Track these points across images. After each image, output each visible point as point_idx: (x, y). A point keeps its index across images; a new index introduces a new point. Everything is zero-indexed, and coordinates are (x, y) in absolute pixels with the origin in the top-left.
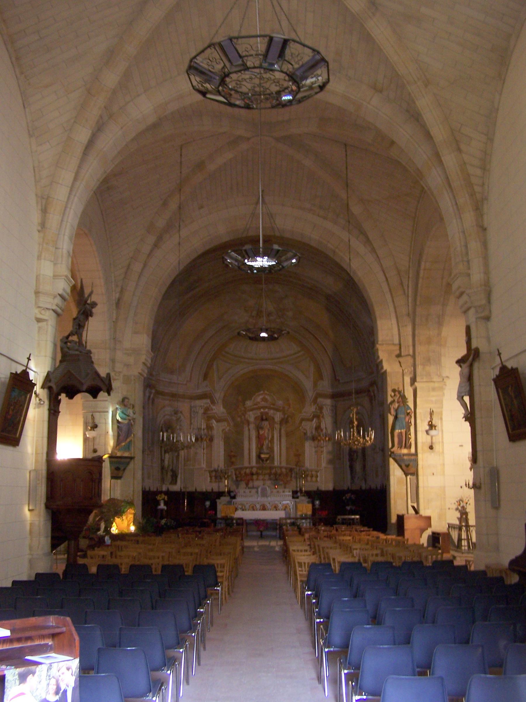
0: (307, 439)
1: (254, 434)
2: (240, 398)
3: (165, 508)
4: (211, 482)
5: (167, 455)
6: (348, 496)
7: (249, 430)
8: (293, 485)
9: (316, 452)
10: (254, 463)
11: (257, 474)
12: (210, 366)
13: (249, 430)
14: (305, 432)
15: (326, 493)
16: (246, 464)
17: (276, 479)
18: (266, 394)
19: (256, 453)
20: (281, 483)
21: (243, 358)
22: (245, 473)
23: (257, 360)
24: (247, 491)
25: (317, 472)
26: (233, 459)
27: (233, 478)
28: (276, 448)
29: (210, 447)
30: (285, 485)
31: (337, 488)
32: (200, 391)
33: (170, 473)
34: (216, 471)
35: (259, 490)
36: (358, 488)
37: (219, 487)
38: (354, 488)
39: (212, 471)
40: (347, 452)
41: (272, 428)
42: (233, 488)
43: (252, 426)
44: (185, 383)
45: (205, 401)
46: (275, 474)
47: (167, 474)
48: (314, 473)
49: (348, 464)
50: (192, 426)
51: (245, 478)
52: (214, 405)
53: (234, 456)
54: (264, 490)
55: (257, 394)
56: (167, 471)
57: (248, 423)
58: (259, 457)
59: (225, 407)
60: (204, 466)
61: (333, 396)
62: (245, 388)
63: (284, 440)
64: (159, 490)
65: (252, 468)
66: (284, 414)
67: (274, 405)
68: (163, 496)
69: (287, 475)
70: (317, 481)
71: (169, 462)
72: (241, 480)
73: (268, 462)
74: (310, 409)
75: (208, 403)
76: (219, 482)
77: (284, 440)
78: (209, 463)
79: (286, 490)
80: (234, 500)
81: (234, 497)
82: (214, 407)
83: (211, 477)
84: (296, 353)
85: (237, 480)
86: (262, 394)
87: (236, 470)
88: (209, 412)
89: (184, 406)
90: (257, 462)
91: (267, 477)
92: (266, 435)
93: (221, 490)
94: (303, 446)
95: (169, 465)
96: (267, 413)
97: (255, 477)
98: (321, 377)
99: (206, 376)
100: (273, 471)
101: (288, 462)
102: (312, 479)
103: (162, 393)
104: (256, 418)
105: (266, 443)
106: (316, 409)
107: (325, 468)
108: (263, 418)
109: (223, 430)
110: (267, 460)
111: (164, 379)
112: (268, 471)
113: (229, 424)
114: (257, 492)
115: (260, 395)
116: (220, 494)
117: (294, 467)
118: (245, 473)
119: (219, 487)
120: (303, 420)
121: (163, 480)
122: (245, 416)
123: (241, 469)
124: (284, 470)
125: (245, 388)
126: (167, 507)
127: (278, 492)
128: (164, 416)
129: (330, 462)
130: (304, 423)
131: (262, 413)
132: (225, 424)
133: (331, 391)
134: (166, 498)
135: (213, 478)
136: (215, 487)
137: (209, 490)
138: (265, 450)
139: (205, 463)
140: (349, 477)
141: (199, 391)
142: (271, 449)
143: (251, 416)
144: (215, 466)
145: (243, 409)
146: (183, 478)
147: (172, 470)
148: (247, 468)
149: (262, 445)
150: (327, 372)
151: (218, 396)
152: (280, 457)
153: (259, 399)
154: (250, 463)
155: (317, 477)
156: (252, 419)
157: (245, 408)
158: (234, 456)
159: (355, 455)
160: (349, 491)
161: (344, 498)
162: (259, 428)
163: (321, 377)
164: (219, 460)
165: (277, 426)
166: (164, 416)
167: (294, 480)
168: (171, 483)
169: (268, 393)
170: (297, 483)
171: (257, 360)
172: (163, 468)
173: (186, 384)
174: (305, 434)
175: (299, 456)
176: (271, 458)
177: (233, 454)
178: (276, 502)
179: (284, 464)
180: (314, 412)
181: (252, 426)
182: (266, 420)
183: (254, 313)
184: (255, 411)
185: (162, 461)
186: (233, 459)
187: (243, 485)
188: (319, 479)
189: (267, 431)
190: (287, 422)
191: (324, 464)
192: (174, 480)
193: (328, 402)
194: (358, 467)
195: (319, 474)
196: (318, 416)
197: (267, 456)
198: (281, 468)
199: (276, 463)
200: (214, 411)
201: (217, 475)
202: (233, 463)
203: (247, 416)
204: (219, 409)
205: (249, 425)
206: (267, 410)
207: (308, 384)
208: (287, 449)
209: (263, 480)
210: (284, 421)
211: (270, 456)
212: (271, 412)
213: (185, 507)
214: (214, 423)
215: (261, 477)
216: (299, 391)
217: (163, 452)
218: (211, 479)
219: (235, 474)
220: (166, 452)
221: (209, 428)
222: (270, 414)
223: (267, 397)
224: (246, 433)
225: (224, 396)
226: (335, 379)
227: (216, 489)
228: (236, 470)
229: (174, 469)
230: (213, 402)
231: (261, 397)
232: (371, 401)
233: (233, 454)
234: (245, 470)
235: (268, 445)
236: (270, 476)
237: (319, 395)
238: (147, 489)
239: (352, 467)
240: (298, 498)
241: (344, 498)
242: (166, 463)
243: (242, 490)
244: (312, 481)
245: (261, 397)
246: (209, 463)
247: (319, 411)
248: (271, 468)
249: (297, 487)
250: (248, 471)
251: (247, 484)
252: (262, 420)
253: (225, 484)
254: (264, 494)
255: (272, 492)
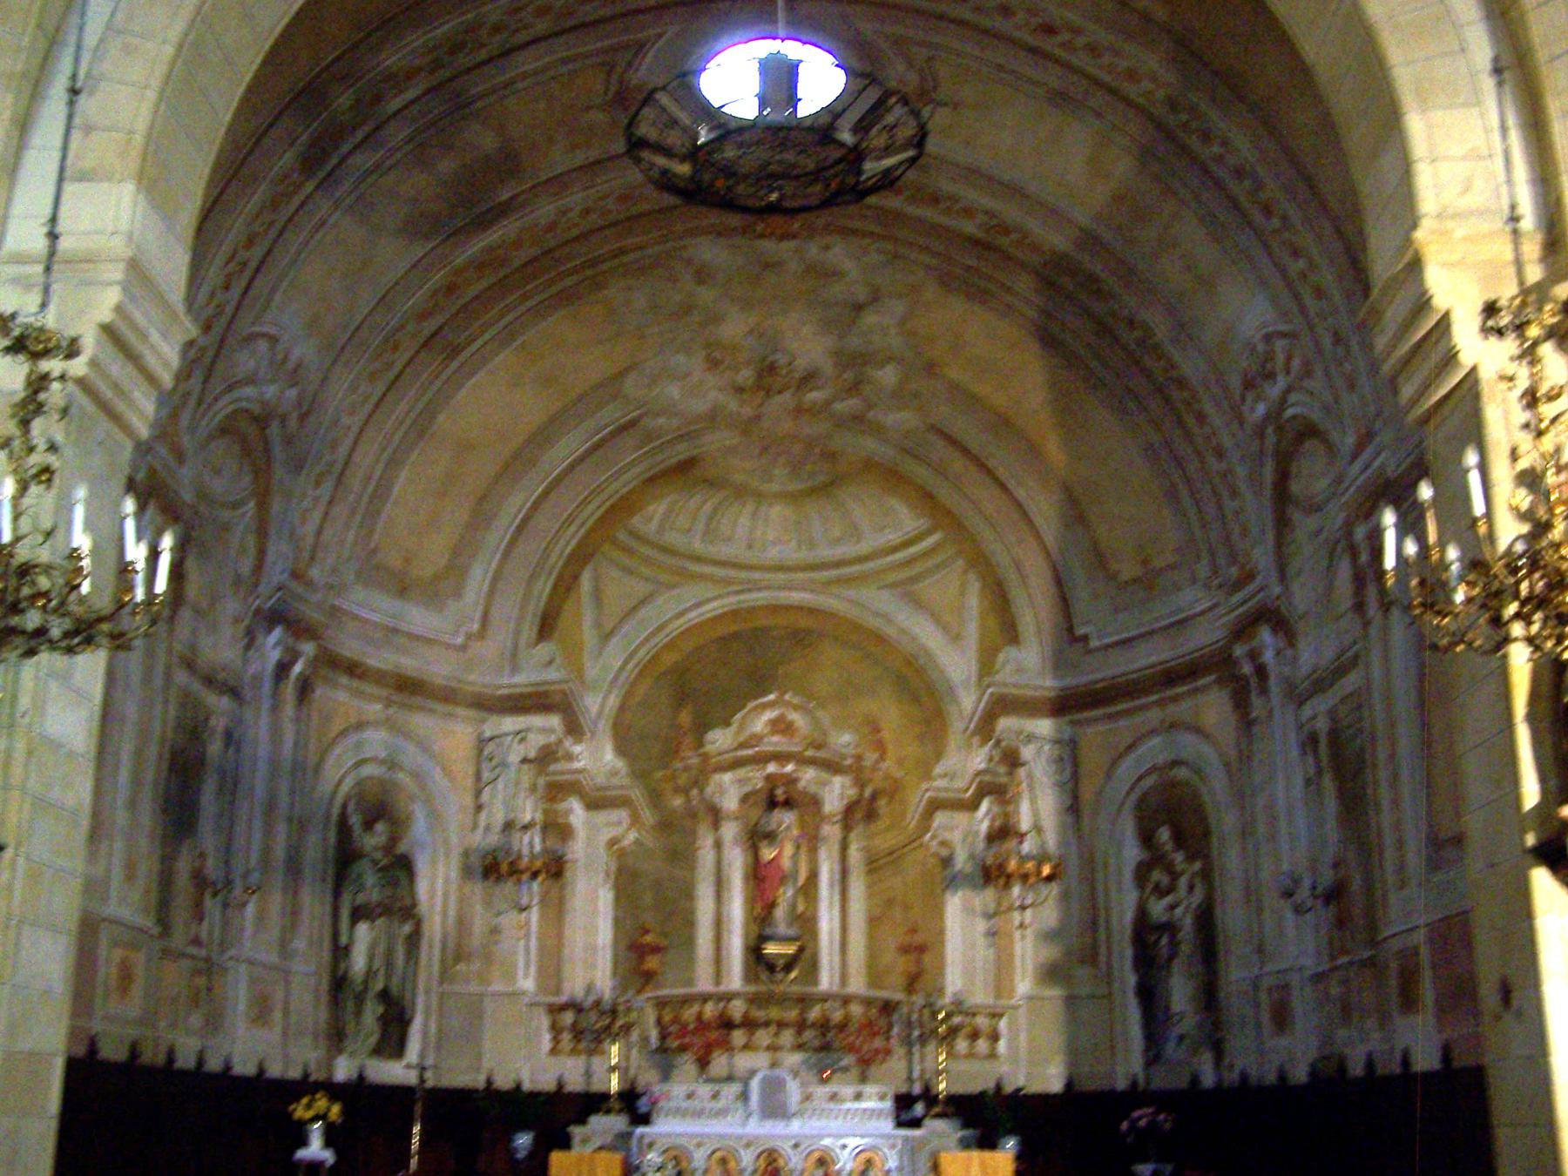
0: (953, 882)
1: (737, 863)
2: (685, 718)
3: (328, 1156)
4: (554, 1051)
5: (363, 929)
6: (1142, 1116)
7: (718, 845)
8: (895, 1072)
9: (992, 934)
10: (735, 979)
11: (750, 1024)
12: (566, 585)
13: (718, 845)
14: (944, 852)
15: (1043, 1101)
16: (704, 984)
17: (825, 1047)
18: (788, 704)
19: (746, 936)
20: (848, 1060)
21: (698, 559)
22: (699, 1017)
23: (750, 568)
24: (705, 1090)
25: (996, 1016)
26: (652, 963)
27: (645, 1039)
28: (827, 922)
29: (556, 909)
30: (865, 1066)
31: (1089, 1085)
32: (523, 679)
33: (372, 1011)
34: (575, 1006)
35: (755, 1084)
36: (1183, 1083)
37: (588, 1074)
38: (1163, 1080)
39: (563, 1008)
40: (1128, 932)
41: (811, 840)
42: (648, 1077)
43: (730, 831)
44: (460, 640)
45: (537, 720)
46: (824, 1026)
47: (358, 1013)
48: (982, 1021)
49: (1132, 979)
50: (483, 816)
51: (699, 1038)
52: (579, 741)
53: (656, 949)
54: (773, 1088)
55: (751, 705)
56: (360, 999)
57: (716, 816)
58: (754, 952)
59: (621, 750)
60: (528, 984)
61: (1064, 705)
62: (703, 682)
63: (857, 888)
64: (317, 1075)
65: (728, 997)
66: (860, 783)
67: (819, 747)
68: (321, 1103)
69: (869, 1028)
70: (992, 1055)
71: (371, 958)
72: (683, 1049)
73: (793, 975)
74: (966, 761)
75: (552, 731)
76: (591, 1053)
77: (857, 888)
78: (551, 964)
79: (870, 1089)
80: (640, 1130)
81: (645, 1119)
82: (577, 749)
83: (556, 1029)
84: (907, 544)
85: (662, 1050)
86: (771, 705)
87: (661, 1004)
88: (561, 766)
89: (454, 735)
90: (750, 976)
91: (787, 1037)
92: (786, 863)
93: (597, 1087)
94: (938, 911)
95: (370, 974)
96: (791, 781)
97: (738, 1037)
98: (1011, 633)
99: (546, 627)
100: (814, 1014)
101: (875, 975)
102: (971, 1046)
103: (354, 669)
104: (745, 799)
105: (785, 895)
106: (991, 759)
107: (1030, 998)
108: (776, 798)
109: (612, 842)
110: (788, 967)
111: (365, 613)
112: (793, 1014)
113: (635, 820)
114: (744, 1096)
115: (765, 706)
116: (594, 1102)
117: (898, 996)
118: (699, 1017)
119: (588, 1074)
120: (935, 806)
121: (337, 1038)
122: (701, 791)
123: (686, 1000)
124: (856, 1009)
125: (703, 682)
126: (339, 1154)
127: (833, 1097)
128: (359, 764)
129: (1051, 973)
130: (940, 818)
131: (769, 778)
132: (622, 814)
133: (1049, 683)
134: (336, 1109)
135: (566, 1037)
136: (571, 1072)
137: (547, 1083)
138: (782, 928)
139: (533, 970)
140: (1136, 1031)
141: (517, 679)
142: (806, 923)
143: (729, 790)
144: (574, 986)
145: (695, 761)
146: (433, 1028)
147: (385, 995)
148: (705, 998)
149: (771, 906)
150: (1034, 610)
151: (597, 704)
152: (842, 955)
153: (760, 724)
154: (718, 976)
155: (995, 1037)
156: (730, 803)
157: (705, 757)
158: (656, 949)
159: (1164, 941)
160: (1135, 1096)
161: (1125, 1125)
162: (756, 837)
163: (1011, 633)
164: (593, 965)
165: (831, 831)
166: (359, 764)
167: (900, 1051)
168: (377, 1052)
169: (796, 700)
170: (910, 1062)
171: (750, 568)
172: (339, 983)
173: (463, 648)
174: (947, 862)
175: (920, 951)
176: (804, 959)
177: (649, 943)
178: (827, 1142)
179: (857, 985)
180: (979, 773)
181: (730, 831)
182: (788, 804)
183: (746, 375)
184: (741, 772)
185: (340, 952)
186: (652, 963)
187: (687, 1065)
188: (1002, 1045)
189: (789, 850)
190: (871, 816)
191: (1024, 985)
192: (392, 1041)
193: (1044, 726)
194: (1180, 992)
195: (1003, 1024)
196: (994, 789)
197: (790, 950)
198: (846, 1001)
199: (826, 980)
200: (577, 765)
201: (586, 1024)
202: (648, 977)
203: (709, 790)
204: (597, 758)
205: (716, 825)
206: (789, 768)
207: (956, 664)
208: (873, 921)
209: (773, 1048)
210: (860, 812)
211: (801, 950)
212: (808, 776)
213: (408, 1157)
214: (576, 813)
215: (763, 1037)
216: (920, 690)
217: (345, 914)
218: (556, 1040)
219: (659, 1022)
220: (358, 914)
221: (557, 829)
222: (801, 784)
223: (795, 717)
224: (706, 857)
225: (622, 708)
226: (1070, 638)
227: (575, 1084)
228: (661, 1004)
229: (395, 990)
230: (574, 728)
231: (769, 715)
232: (1241, 702)
233: (648, 938)
234: (695, 1008)
235: (794, 906)
236: (799, 1032)
237: (1003, 705)
238: (112, 1051)
239: (1150, 996)
240: (916, 1123)
241: (1125, 1125)
242: (359, 961)
243: (682, 1087)
244: (971, 1055)
245: (769, 715)
246: (551, 964)
247: (1002, 769)
248: (804, 1001)
249: (910, 1079)
250: (710, 1010)
251: (703, 1063)
252: (772, 804)
253: (610, 1069)
254: (774, 1108)
255: (807, 1098)
